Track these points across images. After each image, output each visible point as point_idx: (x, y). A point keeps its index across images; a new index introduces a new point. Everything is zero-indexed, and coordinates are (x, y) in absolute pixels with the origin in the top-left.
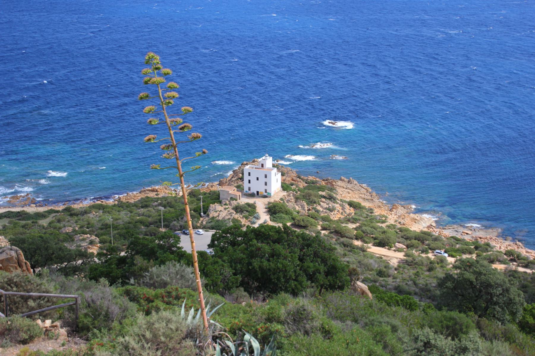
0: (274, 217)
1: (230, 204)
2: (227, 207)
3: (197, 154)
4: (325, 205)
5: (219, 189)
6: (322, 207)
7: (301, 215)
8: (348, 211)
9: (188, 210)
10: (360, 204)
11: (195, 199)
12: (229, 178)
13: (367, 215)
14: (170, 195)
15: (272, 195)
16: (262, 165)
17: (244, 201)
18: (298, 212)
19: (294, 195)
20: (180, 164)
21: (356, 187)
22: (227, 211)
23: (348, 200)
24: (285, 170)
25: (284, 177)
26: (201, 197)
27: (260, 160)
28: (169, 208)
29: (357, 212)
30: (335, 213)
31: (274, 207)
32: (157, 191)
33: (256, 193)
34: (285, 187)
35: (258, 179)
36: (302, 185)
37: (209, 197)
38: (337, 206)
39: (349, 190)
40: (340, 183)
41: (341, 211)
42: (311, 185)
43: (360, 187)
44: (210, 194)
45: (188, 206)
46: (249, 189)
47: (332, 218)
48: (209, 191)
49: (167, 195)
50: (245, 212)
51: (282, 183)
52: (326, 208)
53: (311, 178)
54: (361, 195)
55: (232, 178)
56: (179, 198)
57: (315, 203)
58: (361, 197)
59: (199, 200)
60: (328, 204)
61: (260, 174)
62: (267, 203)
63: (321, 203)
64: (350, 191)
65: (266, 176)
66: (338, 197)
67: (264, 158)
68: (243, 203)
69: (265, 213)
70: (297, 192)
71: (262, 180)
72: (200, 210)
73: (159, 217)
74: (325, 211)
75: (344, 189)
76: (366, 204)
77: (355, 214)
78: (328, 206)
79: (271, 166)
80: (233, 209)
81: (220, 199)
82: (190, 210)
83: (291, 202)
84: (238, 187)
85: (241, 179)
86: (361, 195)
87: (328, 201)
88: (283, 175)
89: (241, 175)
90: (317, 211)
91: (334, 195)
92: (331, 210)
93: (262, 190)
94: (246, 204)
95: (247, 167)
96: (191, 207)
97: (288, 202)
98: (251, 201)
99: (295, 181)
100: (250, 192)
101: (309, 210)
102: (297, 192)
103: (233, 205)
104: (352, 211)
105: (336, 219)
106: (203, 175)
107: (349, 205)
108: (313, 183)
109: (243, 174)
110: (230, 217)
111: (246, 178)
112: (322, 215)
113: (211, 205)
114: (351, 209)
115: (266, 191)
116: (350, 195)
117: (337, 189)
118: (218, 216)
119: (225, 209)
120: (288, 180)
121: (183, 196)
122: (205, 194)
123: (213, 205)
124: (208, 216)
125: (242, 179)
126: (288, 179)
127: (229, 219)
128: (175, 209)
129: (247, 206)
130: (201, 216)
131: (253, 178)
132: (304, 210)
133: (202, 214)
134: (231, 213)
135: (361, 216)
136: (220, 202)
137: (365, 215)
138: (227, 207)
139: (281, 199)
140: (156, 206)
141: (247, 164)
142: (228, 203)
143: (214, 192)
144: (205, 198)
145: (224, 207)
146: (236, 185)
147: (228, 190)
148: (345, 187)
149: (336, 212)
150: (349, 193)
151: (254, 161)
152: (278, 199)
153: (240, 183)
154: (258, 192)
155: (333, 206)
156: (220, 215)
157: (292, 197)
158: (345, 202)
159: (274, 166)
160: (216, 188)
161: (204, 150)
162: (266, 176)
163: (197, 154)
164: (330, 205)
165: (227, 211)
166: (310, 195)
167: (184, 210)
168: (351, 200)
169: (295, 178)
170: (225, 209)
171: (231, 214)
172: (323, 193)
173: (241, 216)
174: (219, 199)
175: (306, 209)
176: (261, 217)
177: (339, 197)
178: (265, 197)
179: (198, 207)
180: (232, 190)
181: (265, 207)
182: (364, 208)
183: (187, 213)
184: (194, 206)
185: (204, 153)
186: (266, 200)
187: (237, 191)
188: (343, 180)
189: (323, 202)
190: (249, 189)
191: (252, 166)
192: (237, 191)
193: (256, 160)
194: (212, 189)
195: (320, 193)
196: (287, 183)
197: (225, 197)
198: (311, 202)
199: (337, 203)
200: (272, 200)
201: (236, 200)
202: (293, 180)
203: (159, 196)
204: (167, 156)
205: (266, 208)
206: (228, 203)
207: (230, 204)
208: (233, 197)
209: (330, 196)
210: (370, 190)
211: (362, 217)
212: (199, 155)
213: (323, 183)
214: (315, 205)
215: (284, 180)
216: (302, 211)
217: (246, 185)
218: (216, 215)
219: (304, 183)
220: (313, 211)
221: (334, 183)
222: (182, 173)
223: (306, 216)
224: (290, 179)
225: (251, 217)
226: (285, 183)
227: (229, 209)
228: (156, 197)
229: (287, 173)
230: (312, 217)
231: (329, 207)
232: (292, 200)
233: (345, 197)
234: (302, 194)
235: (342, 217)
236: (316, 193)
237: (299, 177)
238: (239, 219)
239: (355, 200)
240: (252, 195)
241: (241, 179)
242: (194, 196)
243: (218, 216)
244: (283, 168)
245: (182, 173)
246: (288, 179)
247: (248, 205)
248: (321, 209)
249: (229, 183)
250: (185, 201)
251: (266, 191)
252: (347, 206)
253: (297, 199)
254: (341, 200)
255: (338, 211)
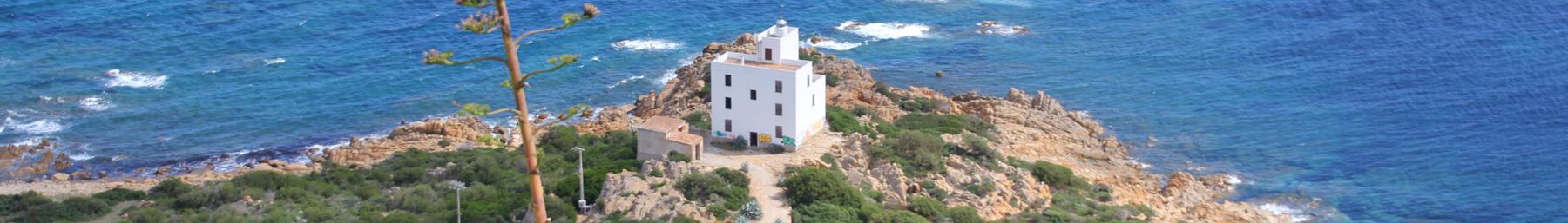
0: (805, 213)
1: (669, 173)
2: (659, 180)
3: (567, 18)
4: (961, 176)
5: (635, 127)
6: (951, 181)
7: (887, 207)
8: (1031, 195)
9: (540, 190)
10: (1068, 172)
11: (560, 157)
12: (667, 93)
13: (1092, 205)
14: (484, 145)
15: (798, 143)
16: (768, 54)
17: (710, 162)
18: (878, 198)
19: (864, 145)
20: (515, 49)
21: (1056, 120)
22: (658, 194)
23: (1032, 159)
24: (837, 67)
25: (835, 91)
26: (581, 150)
27: (761, 36)
28: (480, 185)
29: (1061, 197)
30: (993, 199)
31: (805, 180)
32: (443, 132)
33: (748, 138)
34: (837, 120)
35: (753, 95)
36: (891, 113)
37: (602, 151)
38: (997, 177)
39: (1034, 131)
40: (1006, 108)
41: (1010, 193)
42: (919, 114)
43: (1069, 121)
44: (606, 141)
45: (538, 179)
46: (728, 127)
47: (982, 215)
48: (602, 134)
49: (473, 146)
50: (714, 196)
51: (828, 107)
52: (964, 186)
53: (917, 92)
54: (1071, 145)
55: (675, 91)
56: (512, 155)
57: (930, 168)
58: (1072, 152)
59: (573, 159)
60: (970, 173)
61: (762, 78)
62: (782, 169)
63: (950, 170)
64: (1039, 133)
65: (779, 88)
66: (1000, 150)
67: (772, 30)
68: (709, 169)
69: (775, 198)
70: (873, 137)
71: (768, 97)
72: (578, 190)
73: (449, 213)
74: (960, 192)
75: (1021, 128)
76: (1089, 173)
77: (1053, 202)
78: (969, 179)
79: (795, 56)
80: (677, 187)
81: (639, 158)
82: (547, 192)
83: (857, 165)
84: (694, 120)
85: (701, 95)
86: (1071, 145)
87: (970, 163)
88: (830, 83)
89: (702, 83)
90: (938, 194)
91: (990, 145)
92: (981, 190)
93: (766, 130)
94: (718, 172)
95: (721, 59)
96: (548, 180)
97: (846, 167)
98: (733, 162)
99: (867, 101)
100: (729, 136)
101: (912, 190)
102: (873, 137)
103: (677, 175)
104: (1045, 192)
105: (994, 218)
106: (586, 84)
107: (1034, 174)
108: (924, 108)
109: (708, 80)
110: (667, 212)
111: (718, 92)
112: (953, 205)
113: (611, 175)
114: (1043, 186)
115: (779, 133)
116: (1037, 145)
117: (999, 127)
118: (632, 209)
119: (653, 187)
120: (848, 97)
121: (524, 150)
122: (591, 141)
123: (617, 176)
124: (601, 208)
125: (705, 95)
126: (847, 95)
127: (666, 218)
128: (499, 187)
129: (721, 179)
130: (579, 210)
131: (738, 93)
132: (898, 191)
133: (583, 202)
134: (671, 200)
135: (1073, 208)
136: (638, 167)
137: (1084, 207)
138: (659, 180)
139: (827, 157)
140: (440, 178)
141: (720, 50)
142: (662, 168)
143: (621, 136)
144: (591, 153)
145: (651, 180)
146: (686, 113)
147: (661, 129)
148: (1023, 119)
149: (995, 196)
150: (1035, 139)
151: (742, 41)
152: (815, 158)
153: (700, 108)
154: (754, 136)
155: (986, 180)
156: (638, 207)
157: (860, 152)
158: (1023, 165)
159: (803, 55)
160: (625, 121)
161: (588, 6)
162: (779, 88)
163: (567, 18)
164: (978, 176)
165: (658, 194)
166: (914, 145)
167: (528, 190)
168: (1043, 158)
169: (867, 93)
170: (653, 187)
171: (671, 202)
172: (956, 140)
173: (703, 209)
174: (634, 157)
175: (904, 187)
176: (764, 211)
177: (1003, 151)
178: (777, 150)
179: (569, 182)
180: (675, 131)
181: (776, 181)
182: (1081, 183)
183: (536, 201)
184: (557, 179)
185: (588, 14)
186: (780, 161)
187: (691, 131)
188: (1018, 100)
189: (956, 166)
190: (728, 127)
191: (738, 56)
192: (691, 131)
193: (748, 36)
194: (612, 126)
195: (947, 138)
196: (845, 106)
197: (652, 151)
198: (918, 167)
199: (1000, 170)
200: (797, 160)
201: (687, 160)
202: (862, 98)
203: (451, 148)
204: (476, 25)
205: (779, 185)
206: (662, 168)
207: (669, 173)
208: (679, 150)
209: (977, 148)
210: (1101, 130)
211: (1075, 211)
212: (573, 22)
213: (956, 108)
214: (930, 175)
215: (835, 99)
216: (890, 193)
217: (717, 115)
218: (624, 204)
219: (897, 108)
220: (925, 193)
221: (989, 109)
222: (520, 76)
223: (900, 206)
224: (852, 95)
225: (733, 213)
226: (838, 109)
227: (664, 188)
228: (439, 149)
229: (846, 76)
230: (920, 213)
231: (975, 181)
232: (860, 161)
233: (1022, 150)
234: (892, 141)
235: (1014, 211)
236: (935, 138)
237: (882, 91)
238: (697, 217)
239: (1054, 160)
240: (737, 146)
241: (701, 95)
242: (559, 147)
243: (632, 209)
244: (830, 63)
245: (520, 76)
246: (847, 95)
247: (725, 174)
248: (949, 189)
249: (666, 109)
250: (529, 162)
251: (779, 133)
252: (1029, 179)
253: (874, 157)
254: (1011, 161)
255: (1002, 194)
